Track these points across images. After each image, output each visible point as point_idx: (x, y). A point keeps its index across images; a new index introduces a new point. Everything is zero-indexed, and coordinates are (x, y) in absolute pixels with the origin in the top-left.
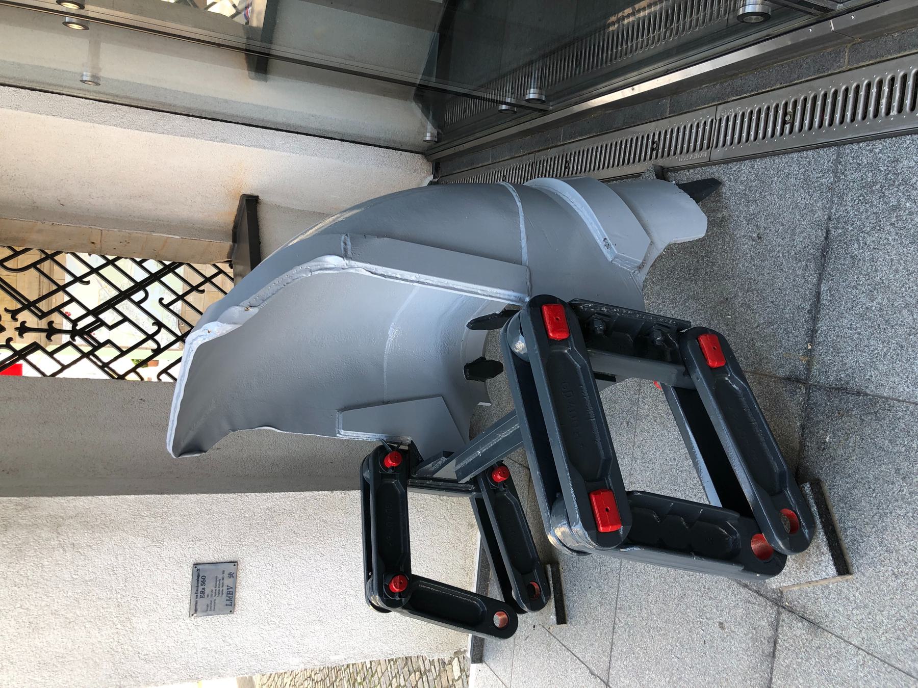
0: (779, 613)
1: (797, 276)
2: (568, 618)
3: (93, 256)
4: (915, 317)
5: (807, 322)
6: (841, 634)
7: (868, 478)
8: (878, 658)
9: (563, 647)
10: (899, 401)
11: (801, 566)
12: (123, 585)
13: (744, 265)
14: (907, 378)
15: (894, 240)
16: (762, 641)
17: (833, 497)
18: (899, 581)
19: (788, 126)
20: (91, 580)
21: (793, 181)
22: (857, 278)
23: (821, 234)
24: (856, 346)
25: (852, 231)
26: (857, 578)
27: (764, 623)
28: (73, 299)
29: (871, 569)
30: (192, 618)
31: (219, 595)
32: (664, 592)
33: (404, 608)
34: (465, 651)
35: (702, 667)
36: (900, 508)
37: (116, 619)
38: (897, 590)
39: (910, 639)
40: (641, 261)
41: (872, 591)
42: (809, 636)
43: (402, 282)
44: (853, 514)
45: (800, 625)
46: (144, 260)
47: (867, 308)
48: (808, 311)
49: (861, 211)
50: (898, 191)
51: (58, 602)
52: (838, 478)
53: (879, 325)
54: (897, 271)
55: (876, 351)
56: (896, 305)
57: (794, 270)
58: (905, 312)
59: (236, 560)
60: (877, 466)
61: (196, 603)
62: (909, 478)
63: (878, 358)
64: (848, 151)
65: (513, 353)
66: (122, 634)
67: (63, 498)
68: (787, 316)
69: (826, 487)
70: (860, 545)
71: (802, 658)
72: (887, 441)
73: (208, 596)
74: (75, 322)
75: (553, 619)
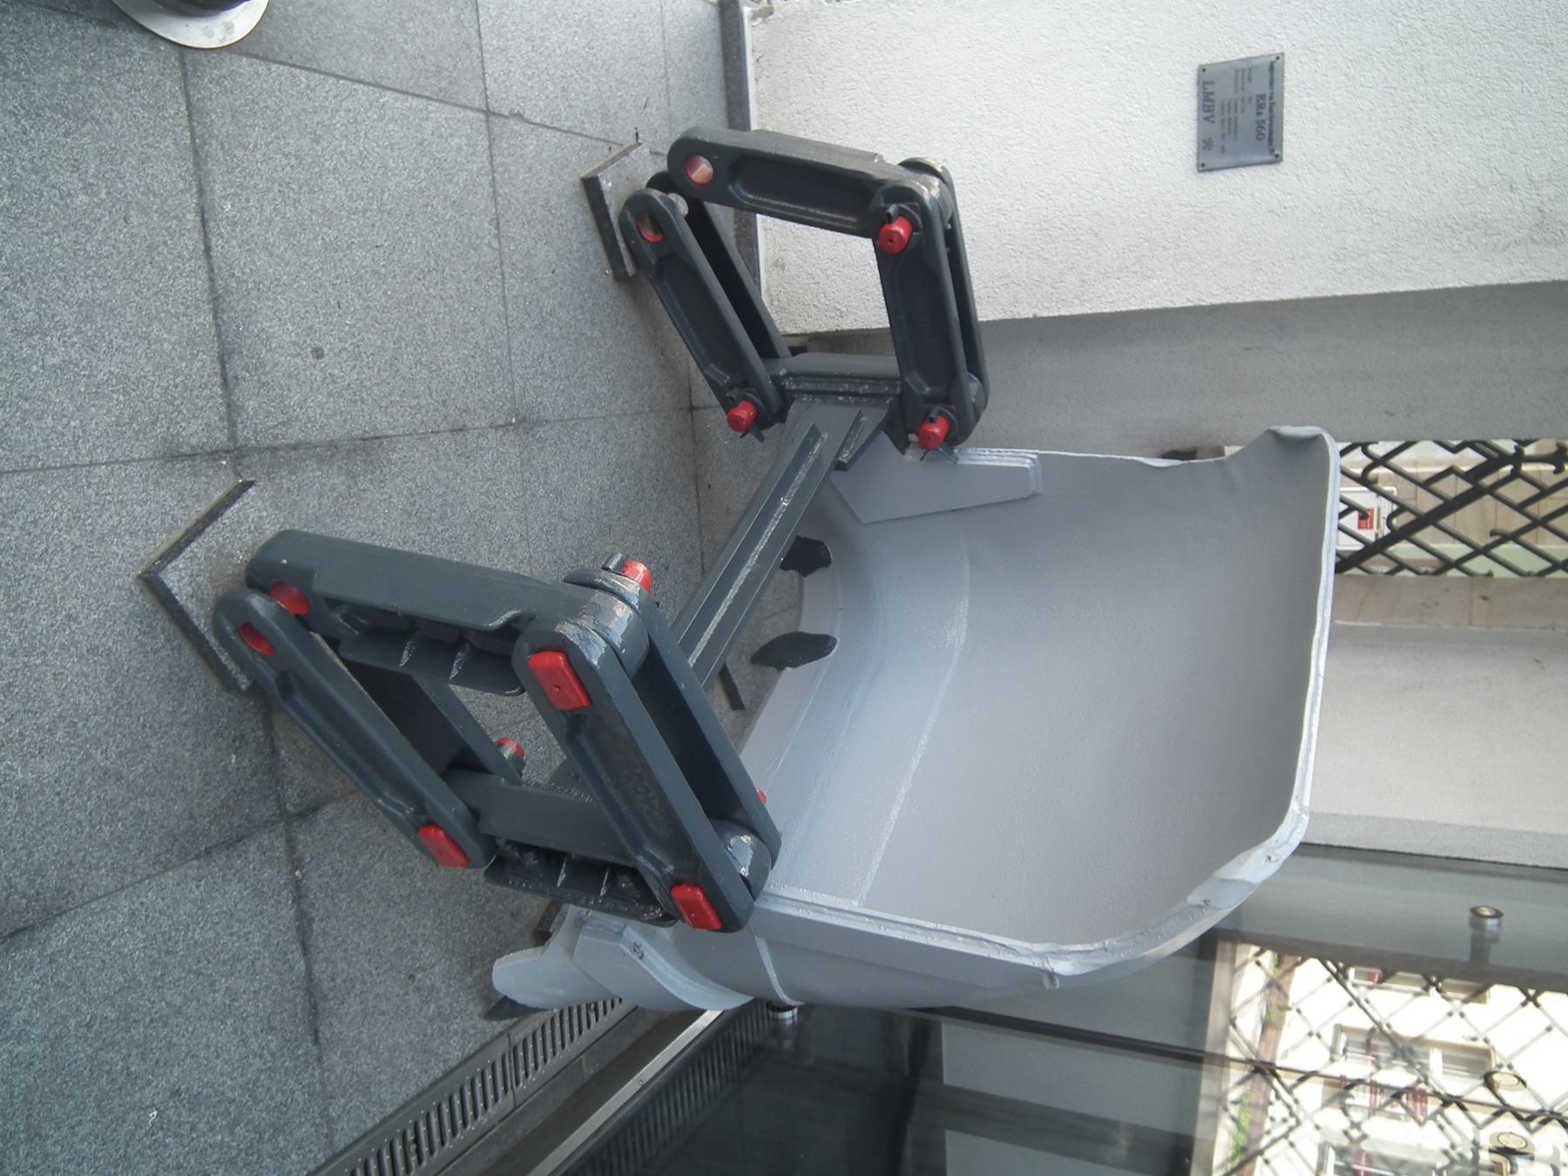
0: (233, 437)
1: (344, 958)
2: (579, 189)
3: (1485, 571)
4: (163, 1003)
5: (312, 905)
6: (125, 470)
7: (158, 740)
8: (55, 468)
9: (578, 130)
10: (148, 877)
11: (219, 553)
12: (1417, 111)
13: (424, 926)
14: (147, 916)
15: (224, 1084)
16: (247, 371)
17: (201, 676)
18: (64, 613)
19: (410, 1137)
20: (1477, 118)
21: (384, 1077)
22: (258, 1006)
23: (325, 1032)
24: (232, 914)
25: (285, 1062)
26: (129, 575)
27: (251, 405)
28: (1520, 508)
29: (112, 603)
30: (1278, 51)
31: (1229, 103)
32: (427, 347)
33: (879, 183)
34: (754, 18)
35: (332, 258)
36: (98, 726)
37: (1428, 40)
38: (62, 598)
39: (16, 533)
40: (581, 937)
41: (99, 570)
42: (174, 433)
43: (954, 929)
44: (163, 671)
45: (194, 441)
46: (1392, 573)
47: (232, 975)
48: (314, 920)
49: (279, 1094)
50: (238, 1146)
51: (1541, 69)
52: (202, 711)
53: (209, 963)
54: (207, 1047)
55: (201, 925)
56: (194, 1003)
57: (349, 964)
58: (179, 1000)
59: (1202, 175)
60: (151, 765)
61: (1271, 83)
62: (100, 777)
63: (195, 918)
64: (319, 1156)
65: (752, 831)
66: (1414, 10)
67: (1532, 280)
68: (342, 896)
69: (215, 685)
70: (139, 630)
71: (176, 386)
72: (147, 809)
73: (1250, 99)
74: (1516, 474)
75: (607, 182)
